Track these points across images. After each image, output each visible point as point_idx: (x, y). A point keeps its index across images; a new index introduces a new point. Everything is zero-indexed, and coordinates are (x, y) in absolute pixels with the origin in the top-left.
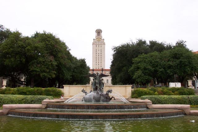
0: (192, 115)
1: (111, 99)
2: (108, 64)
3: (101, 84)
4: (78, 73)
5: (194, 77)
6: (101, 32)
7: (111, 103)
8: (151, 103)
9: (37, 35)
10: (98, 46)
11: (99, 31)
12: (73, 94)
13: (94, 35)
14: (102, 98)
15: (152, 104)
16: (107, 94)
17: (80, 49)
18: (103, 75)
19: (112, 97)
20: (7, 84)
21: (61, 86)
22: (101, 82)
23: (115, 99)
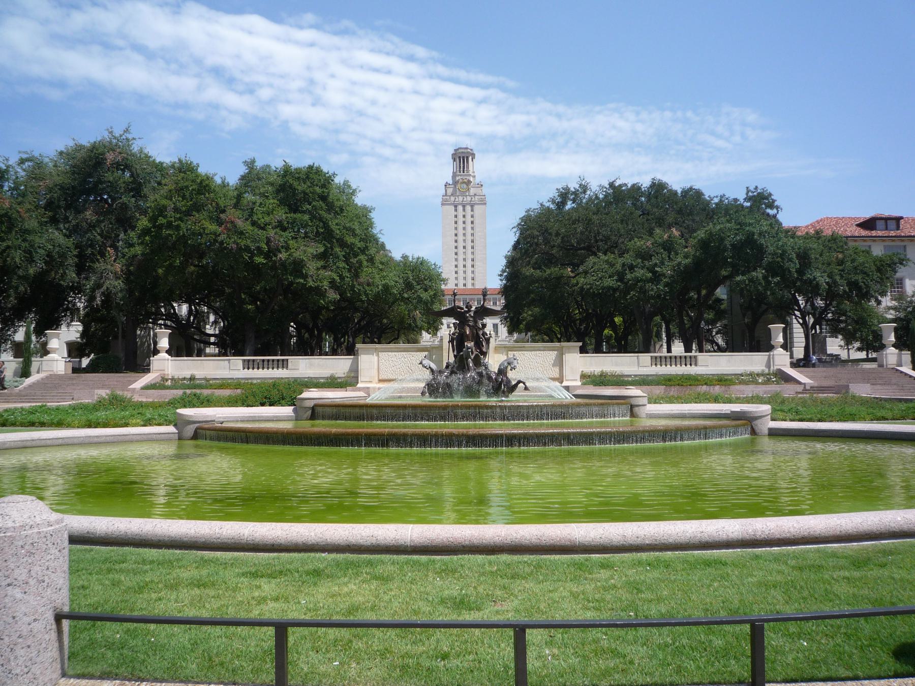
0: (131, 441)
1: (513, 388)
2: (491, 276)
3: (481, 341)
4: (385, 308)
5: (795, 315)
6: (470, 158)
7: (517, 398)
8: (645, 401)
9: (185, 169)
10: (460, 208)
11: (465, 155)
12: (389, 374)
13: (446, 171)
14: (487, 386)
15: (650, 403)
16: (502, 372)
17: (410, 225)
18: (484, 312)
19: (519, 382)
20: (170, 344)
21: (119, 350)
22: (481, 332)
23: (526, 388)
